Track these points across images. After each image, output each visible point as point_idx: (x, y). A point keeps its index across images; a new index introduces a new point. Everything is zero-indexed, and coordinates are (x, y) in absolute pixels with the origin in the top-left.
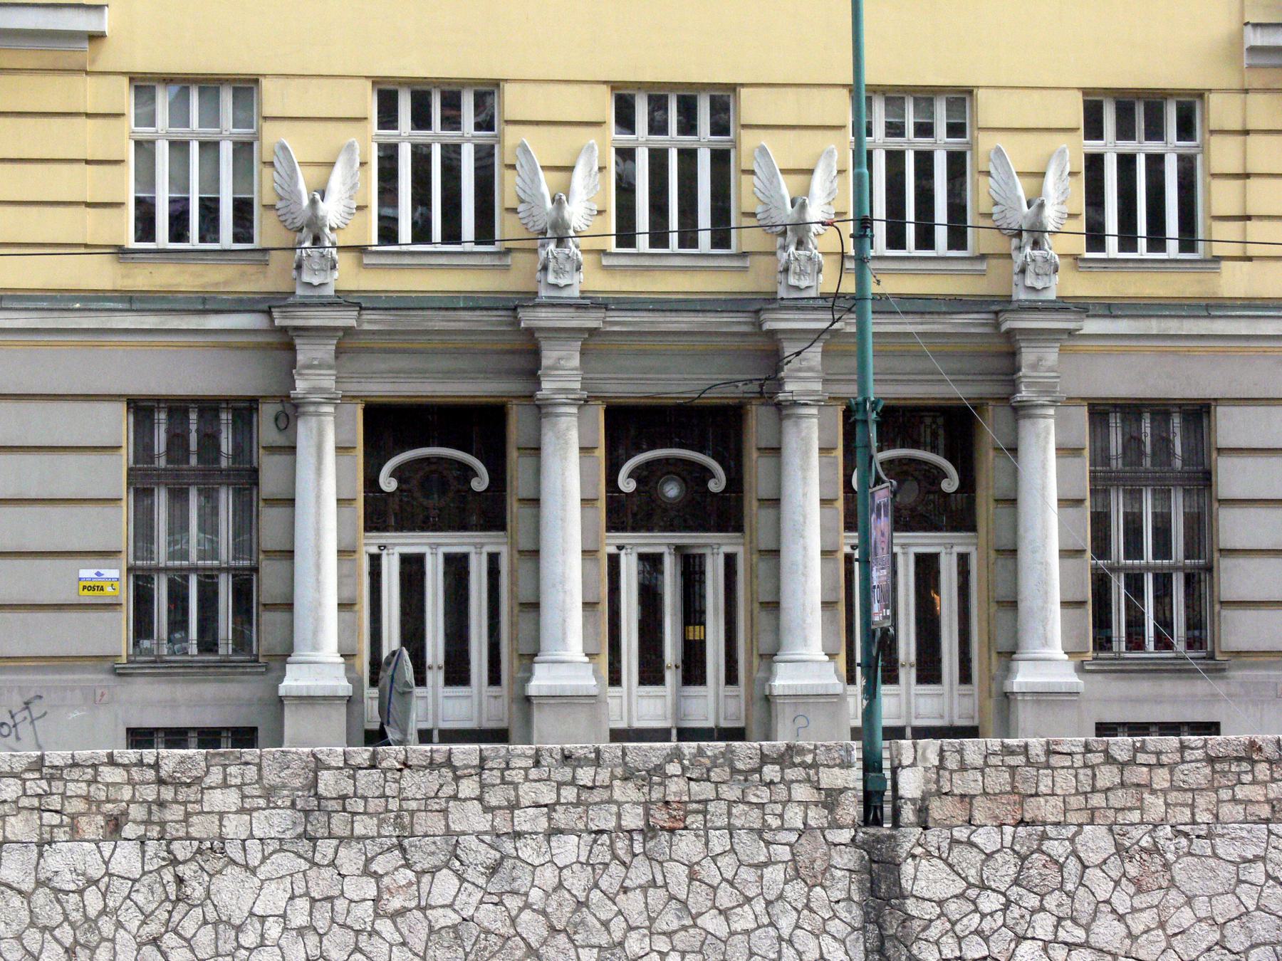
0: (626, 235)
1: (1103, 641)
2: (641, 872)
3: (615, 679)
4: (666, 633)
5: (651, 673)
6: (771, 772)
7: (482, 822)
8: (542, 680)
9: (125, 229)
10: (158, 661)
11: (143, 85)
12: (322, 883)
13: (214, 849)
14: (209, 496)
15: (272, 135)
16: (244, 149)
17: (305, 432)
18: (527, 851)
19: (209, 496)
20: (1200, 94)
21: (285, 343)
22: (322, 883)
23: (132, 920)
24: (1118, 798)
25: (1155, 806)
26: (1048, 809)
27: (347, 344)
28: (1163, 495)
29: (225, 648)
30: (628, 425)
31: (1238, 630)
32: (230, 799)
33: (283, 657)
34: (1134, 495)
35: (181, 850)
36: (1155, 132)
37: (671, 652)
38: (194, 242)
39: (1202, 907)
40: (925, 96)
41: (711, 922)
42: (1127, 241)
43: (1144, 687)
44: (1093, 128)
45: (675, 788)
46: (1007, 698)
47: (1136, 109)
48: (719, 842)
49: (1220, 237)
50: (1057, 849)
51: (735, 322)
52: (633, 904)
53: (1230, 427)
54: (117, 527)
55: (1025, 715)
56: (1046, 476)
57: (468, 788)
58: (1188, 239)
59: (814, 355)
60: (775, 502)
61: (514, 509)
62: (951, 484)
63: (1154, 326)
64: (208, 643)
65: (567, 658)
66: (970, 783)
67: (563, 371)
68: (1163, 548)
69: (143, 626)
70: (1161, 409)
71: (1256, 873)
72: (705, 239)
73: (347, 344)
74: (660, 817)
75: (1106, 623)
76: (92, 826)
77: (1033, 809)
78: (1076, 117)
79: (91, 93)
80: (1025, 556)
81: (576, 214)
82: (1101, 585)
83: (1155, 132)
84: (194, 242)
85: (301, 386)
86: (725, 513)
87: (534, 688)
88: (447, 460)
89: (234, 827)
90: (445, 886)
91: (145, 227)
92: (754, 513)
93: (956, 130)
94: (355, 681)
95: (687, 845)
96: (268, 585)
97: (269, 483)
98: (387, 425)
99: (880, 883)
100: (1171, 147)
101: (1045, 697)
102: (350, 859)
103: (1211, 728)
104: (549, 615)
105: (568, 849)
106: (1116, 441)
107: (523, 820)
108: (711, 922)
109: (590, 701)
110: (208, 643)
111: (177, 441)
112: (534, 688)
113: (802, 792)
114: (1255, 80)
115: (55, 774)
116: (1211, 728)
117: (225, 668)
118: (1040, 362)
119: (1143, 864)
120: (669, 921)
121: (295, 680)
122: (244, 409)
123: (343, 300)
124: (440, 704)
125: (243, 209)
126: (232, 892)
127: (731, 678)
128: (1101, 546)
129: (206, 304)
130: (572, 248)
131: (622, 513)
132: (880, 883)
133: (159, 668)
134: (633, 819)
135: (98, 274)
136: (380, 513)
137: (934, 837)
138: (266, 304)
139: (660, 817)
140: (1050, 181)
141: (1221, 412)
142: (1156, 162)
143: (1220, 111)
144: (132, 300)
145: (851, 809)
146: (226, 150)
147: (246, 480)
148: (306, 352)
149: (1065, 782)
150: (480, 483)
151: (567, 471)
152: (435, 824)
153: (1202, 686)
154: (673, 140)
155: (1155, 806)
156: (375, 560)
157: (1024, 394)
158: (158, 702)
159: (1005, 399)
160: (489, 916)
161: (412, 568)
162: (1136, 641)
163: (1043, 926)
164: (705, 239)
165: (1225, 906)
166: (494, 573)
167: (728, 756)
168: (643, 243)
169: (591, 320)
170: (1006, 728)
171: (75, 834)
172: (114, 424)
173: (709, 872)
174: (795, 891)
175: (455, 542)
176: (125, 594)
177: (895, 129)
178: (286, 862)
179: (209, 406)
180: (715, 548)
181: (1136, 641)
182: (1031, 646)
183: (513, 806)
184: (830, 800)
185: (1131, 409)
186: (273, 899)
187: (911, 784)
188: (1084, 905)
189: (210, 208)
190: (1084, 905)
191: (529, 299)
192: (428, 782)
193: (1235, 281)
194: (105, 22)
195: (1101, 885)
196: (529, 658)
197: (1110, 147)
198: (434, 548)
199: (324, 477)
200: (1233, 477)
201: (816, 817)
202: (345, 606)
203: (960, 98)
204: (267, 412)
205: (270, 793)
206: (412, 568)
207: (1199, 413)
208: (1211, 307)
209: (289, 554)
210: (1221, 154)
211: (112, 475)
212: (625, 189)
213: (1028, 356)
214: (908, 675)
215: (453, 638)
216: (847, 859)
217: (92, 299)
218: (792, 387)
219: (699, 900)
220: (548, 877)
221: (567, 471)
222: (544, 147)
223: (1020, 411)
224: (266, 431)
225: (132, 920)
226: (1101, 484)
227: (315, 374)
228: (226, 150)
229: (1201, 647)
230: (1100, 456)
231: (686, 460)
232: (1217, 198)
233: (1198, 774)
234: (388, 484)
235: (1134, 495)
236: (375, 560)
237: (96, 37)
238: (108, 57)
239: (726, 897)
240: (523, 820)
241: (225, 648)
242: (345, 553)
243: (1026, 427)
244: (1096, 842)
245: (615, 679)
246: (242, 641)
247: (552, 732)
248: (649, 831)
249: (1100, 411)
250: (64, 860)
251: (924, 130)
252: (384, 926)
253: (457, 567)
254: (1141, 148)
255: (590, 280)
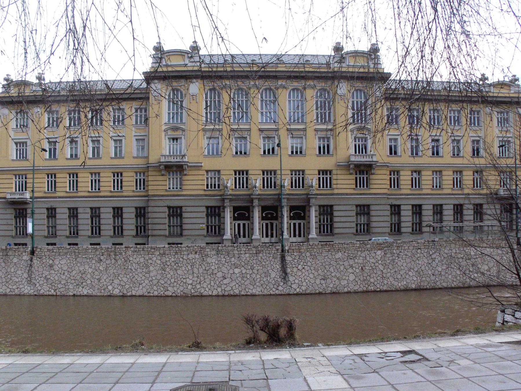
0: (264, 187)
1: (320, 232)
2: (255, 258)
3: (263, 237)
4: (268, 232)
5: (295, 236)
6: (270, 247)
7: (237, 252)
8: (254, 237)
9: (431, 187)
10: (209, 235)
11: (207, 171)
12: (219, 259)
13: (207, 255)
14: (215, 217)
15: (222, 177)
16: (219, 178)
17: (226, 210)
18: (242, 256)
19: (215, 217)
20: (332, 170)
21: (223, 200)
22: (219, 259)
23: (198, 263)
24: (311, 249)
25: (315, 250)
26: (303, 251)
27: (231, 200)
28: (327, 216)
29: (217, 234)
30: (264, 209)
31: (336, 231)
32: (208, 250)
33: (224, 235)
34: (324, 216)
35: (203, 255)
36: (327, 174)
37: (269, 234)
38: (213, 189)
39: (320, 261)
40: (299, 171)
41: (263, 263)
42: (296, 187)
43: (325, 237)
44: (319, 174)
45: (259, 249)
46: (252, 240)
47: (324, 172)
48: (264, 254)
49: (334, 186)
50: (304, 255)
51: (248, 197)
52: (254, 261)
53: (335, 208)
54: (205, 221)
55: (310, 240)
56: (313, 214)
57: (236, 249)
58: (398, 187)
59: (286, 200)
60: (253, 217)
61: (306, 217)
62: (302, 215)
63: (326, 197)
64: (215, 233)
65: (257, 234)
66: (294, 248)
67: (256, 203)
68: (327, 222)
69: (208, 231)
70: (327, 206)
71: (326, 257)
72: (273, 187)
73: (231, 200)
74: (258, 252)
75: (321, 231)
76: (193, 253)
77: (301, 251)
78: (317, 172)
79: (201, 172)
80: (311, 223)
81: (257, 185)
82: (320, 225)
83: (327, 174)
84: (213, 189)
85: (225, 205)
86: (276, 218)
87: (253, 238)
88: (242, 213)
89: (209, 253)
90: (233, 259)
91: (207, 187)
92: (251, 219)
93: (303, 175)
94: (232, 238)
95: (261, 255)
96: (222, 227)
97: (222, 214)
98: (235, 209)
99: (283, 258)
100: (328, 176)
101: (312, 239)
102: (222, 256)
103: (181, 244)
104: (254, 230)
105: (247, 255)
106: (322, 210)
107: (242, 252)
108: (263, 263)
109: (260, 239)
110: (215, 233)
111: (211, 211)
112: (253, 238)
113: (274, 249)
114: (338, 168)
115: (189, 247)
116: (181, 244)
117: (217, 236)
118: (313, 201)
119: (314, 257)
120: (259, 263)
121: (225, 237)
122: (219, 207)
123: (230, 195)
124: (242, 240)
125: (219, 185)
126: (209, 260)
127: (276, 237)
128: (320, 221)
129: (214, 196)
130: (314, 188)
131: (263, 218)
132: (283, 258)
133: (210, 236)
134: (254, 252)
135: (202, 193)
136: (235, 219)
137: (289, 254)
138: (221, 195)
139: (258, 252)
140: (258, 181)
141: (371, 206)
142: (327, 178)
143: (334, 172)
144: (206, 195)
145: (280, 251)
146: (217, 178)
147: (219, 215)
148: (226, 201)
149: (305, 248)
150: (247, 215)
151: (257, 214)
152: (232, 253)
153: (331, 237)
154: (269, 176)
155: (315, 250)
156: (235, 224)
157: (311, 204)
158: (209, 240)
159: (252, 205)
160: (238, 262)
161: (239, 225)
162: (324, 232)
163: (302, 263)
164: (273, 187)
165: (323, 261)
166: (248, 225)
167: (266, 245)
168: (266, 188)
169: (259, 197)
170: (308, 242)
171: (192, 254)
172: (204, 209)
173: (263, 258)
174: (273, 260)
175: (299, 221)
176: (206, 228)
177: (295, 175)
178: (215, 257)
179: (215, 207)
180: (275, 222)
181: (324, 232)
182: (311, 233)
183: (241, 251)
184: (277, 250)
185: (324, 206)
186: (213, 261)
187: (287, 248)
188: (307, 261)
189: (215, 185)
190: (307, 261)
191: (252, 194)
192: (231, 248)
193: (336, 191)
194: (203, 165)
195: (309, 259)
196: (252, 235)
197: (321, 176)
198: (241, 223)
199: (228, 215)
200: (335, 214)
201: (276, 252)
202: (231, 229)
203: (303, 171)
204: (222, 208)
205: (213, 249)
206: (239, 225)
207: (331, 206)
208: (55, 197)
209: (224, 223)
210: (334, 177)
211: (388, 213)
212: (292, 183)
213: (311, 200)
214: (297, 236)
215: (301, 232)
216: (279, 256)
217: (201, 195)
218: (283, 204)
219: (262, 261)
220: (245, 258)
221: (257, 214)
222: (310, 177)
223: (310, 206)
224: (221, 210)
225: (198, 263)
226: (320, 214)
227: (227, 203)
228: (217, 178)
229: (122, 235)
230: (320, 211)
231: (271, 212)
232: (334, 182)
233: (320, 247)
234: (236, 215)
235: (324, 216)
236: (235, 224)
237: (202, 166)
238: (203, 168)
239: (265, 261)
240: (242, 252)
241: (217, 234)
242: (231, 223)
243: (311, 208)
244: (308, 254)
245: (290, 237)
246: (219, 233)
247: (255, 244)
248: (256, 253)
249: (320, 206)
250: (190, 256)
251: (299, 175)
252: (226, 264)
253: (300, 224)
254: (325, 176)
255: (288, 192)
